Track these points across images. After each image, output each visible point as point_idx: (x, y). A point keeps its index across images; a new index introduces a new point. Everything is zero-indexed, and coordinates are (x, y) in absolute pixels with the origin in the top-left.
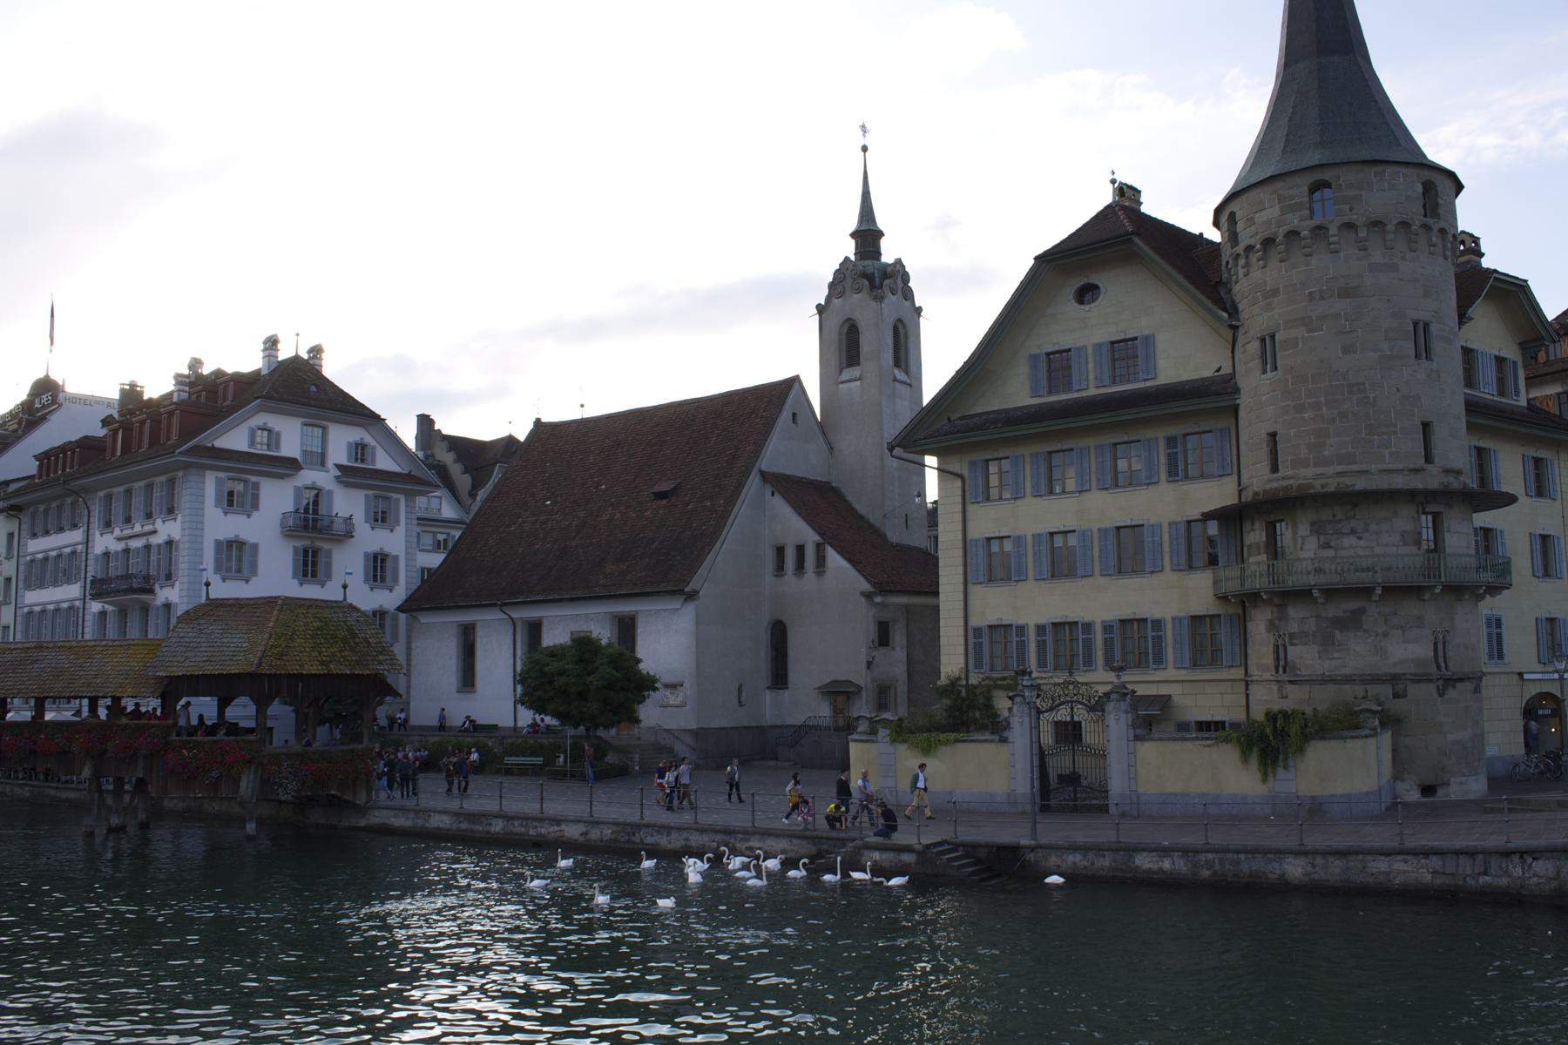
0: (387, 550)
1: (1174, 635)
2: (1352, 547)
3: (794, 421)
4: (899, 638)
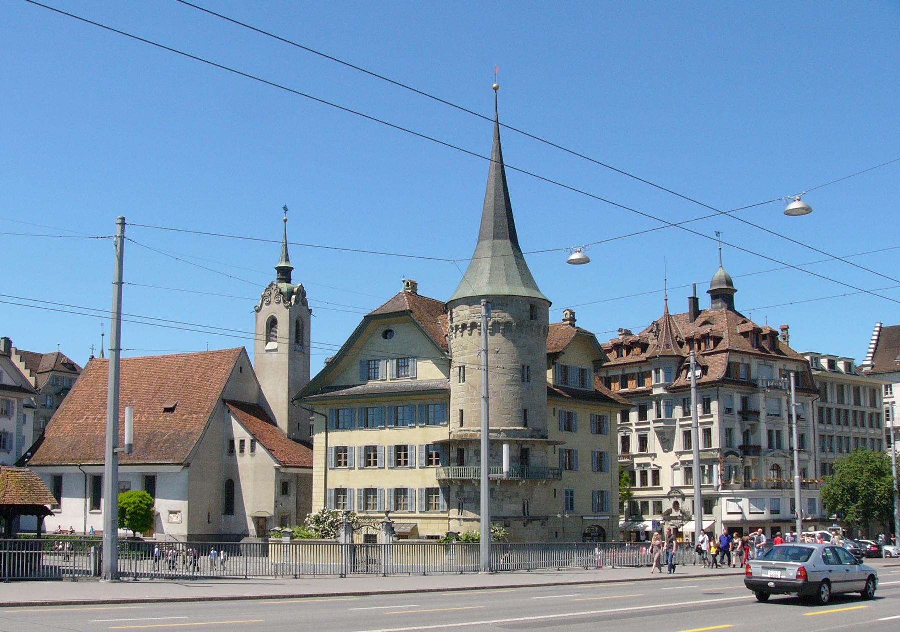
0: (7, 430)
1: (419, 496)
3: (241, 371)
4: (293, 490)
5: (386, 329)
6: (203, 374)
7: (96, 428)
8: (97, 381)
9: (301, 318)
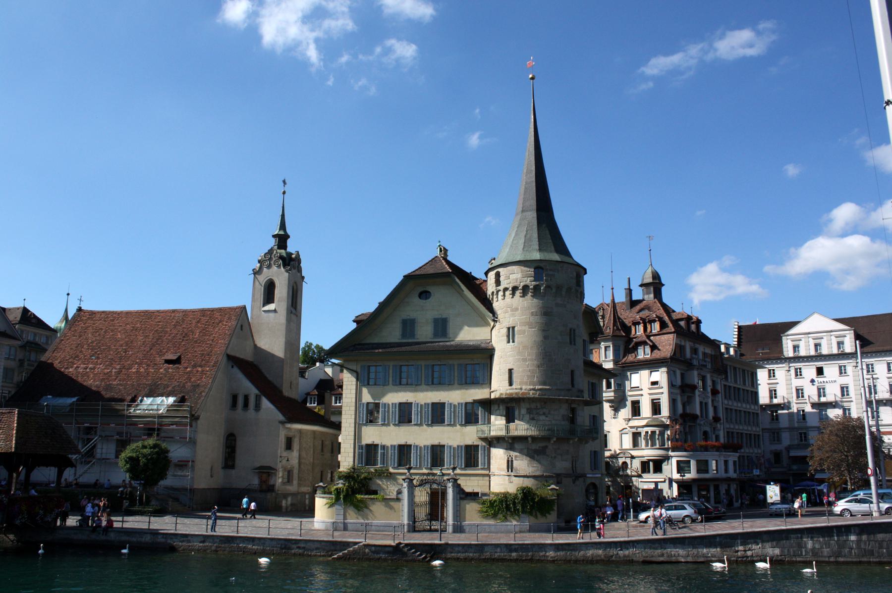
2: (544, 420)
3: (242, 330)
4: (296, 445)
6: (204, 330)
7: (88, 377)
8: (85, 332)
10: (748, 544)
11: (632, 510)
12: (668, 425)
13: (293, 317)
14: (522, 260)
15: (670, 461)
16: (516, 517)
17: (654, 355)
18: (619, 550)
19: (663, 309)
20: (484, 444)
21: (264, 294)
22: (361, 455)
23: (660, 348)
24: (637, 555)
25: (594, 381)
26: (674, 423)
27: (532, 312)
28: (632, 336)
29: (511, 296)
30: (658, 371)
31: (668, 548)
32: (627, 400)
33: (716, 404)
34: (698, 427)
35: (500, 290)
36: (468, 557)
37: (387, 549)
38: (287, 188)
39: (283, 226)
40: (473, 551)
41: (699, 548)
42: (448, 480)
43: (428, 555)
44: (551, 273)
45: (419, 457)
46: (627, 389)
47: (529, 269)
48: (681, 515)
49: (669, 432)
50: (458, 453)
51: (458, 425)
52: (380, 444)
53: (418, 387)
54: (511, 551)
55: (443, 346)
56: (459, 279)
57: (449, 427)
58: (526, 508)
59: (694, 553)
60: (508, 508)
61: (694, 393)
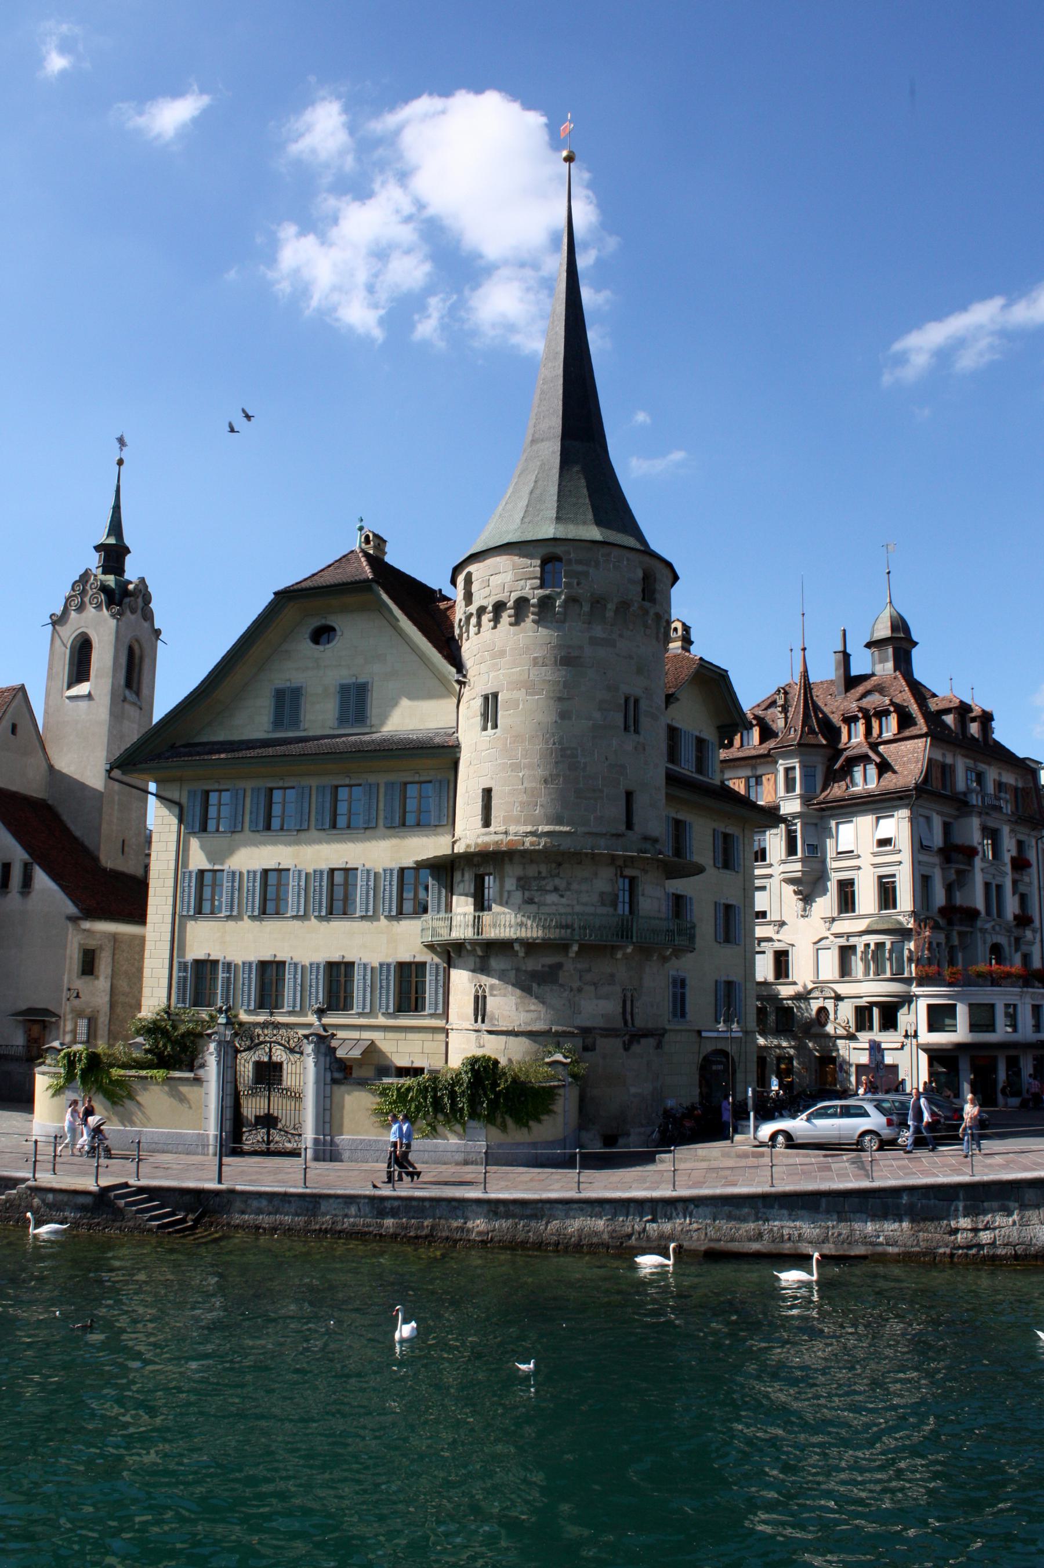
4: (104, 965)
5: (319, 624)
9: (137, 641)
10: (985, 1213)
11: (752, 1114)
12: (911, 929)
13: (131, 711)
14: (514, 540)
15: (913, 1006)
16: (458, 1128)
17: (883, 783)
18: (648, 1221)
19: (911, 690)
20: (437, 960)
21: (71, 664)
22: (183, 981)
23: (896, 768)
24: (695, 1235)
25: (729, 831)
26: (922, 925)
27: (535, 658)
28: (841, 746)
29: (492, 623)
30: (892, 816)
31: (775, 1220)
32: (829, 880)
33: (1022, 889)
34: (979, 935)
35: (471, 614)
36: (281, 1224)
37: (81, 1200)
38: (125, 455)
39: (116, 527)
40: (293, 1210)
41: (854, 1220)
42: (306, 1037)
43: (191, 1217)
44: (580, 568)
45: (299, 988)
46: (829, 856)
47: (529, 562)
48: (855, 1129)
49: (912, 945)
50: (381, 980)
51: (382, 917)
52: (221, 958)
53: (303, 835)
54: (382, 1214)
55: (355, 743)
56: (387, 593)
57: (364, 922)
58: (479, 1107)
59: (840, 1234)
60: (437, 1104)
61: (971, 864)
